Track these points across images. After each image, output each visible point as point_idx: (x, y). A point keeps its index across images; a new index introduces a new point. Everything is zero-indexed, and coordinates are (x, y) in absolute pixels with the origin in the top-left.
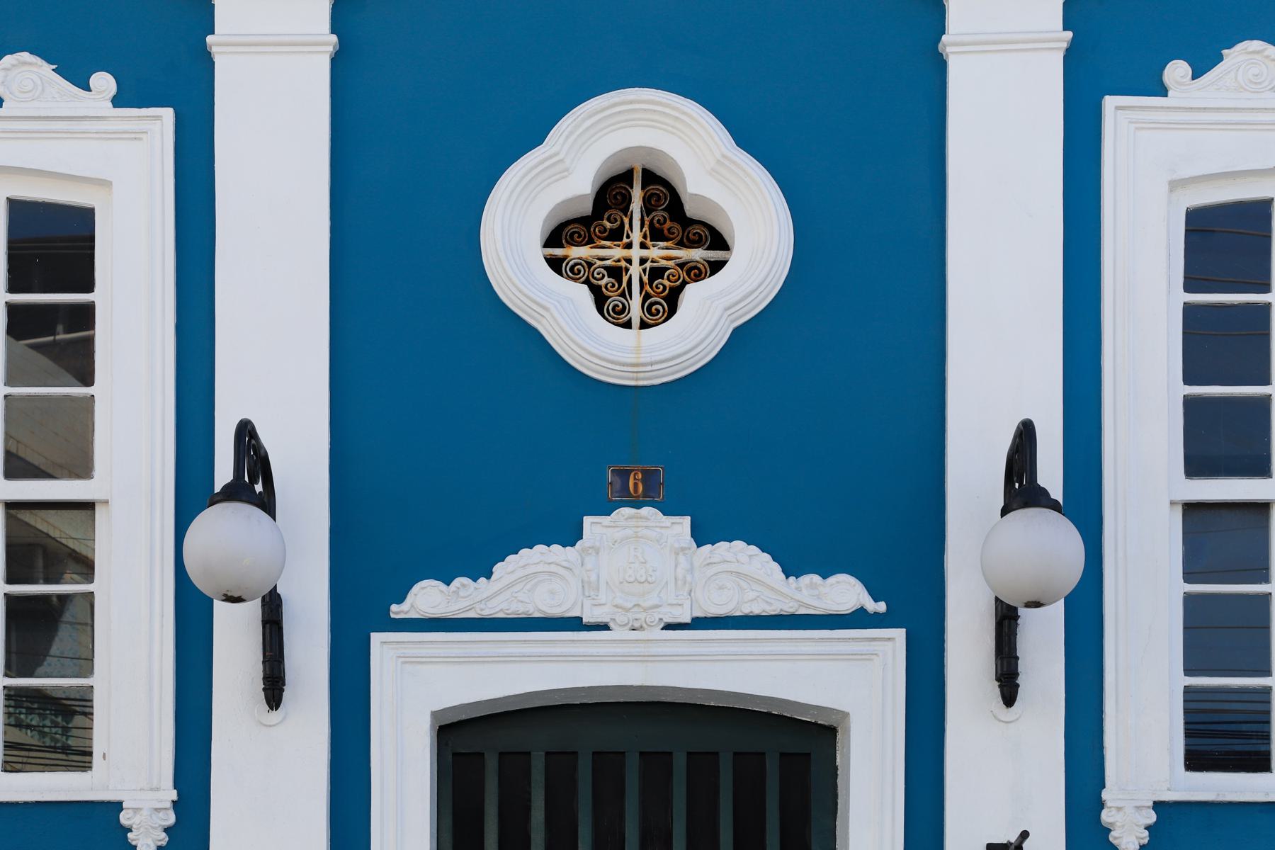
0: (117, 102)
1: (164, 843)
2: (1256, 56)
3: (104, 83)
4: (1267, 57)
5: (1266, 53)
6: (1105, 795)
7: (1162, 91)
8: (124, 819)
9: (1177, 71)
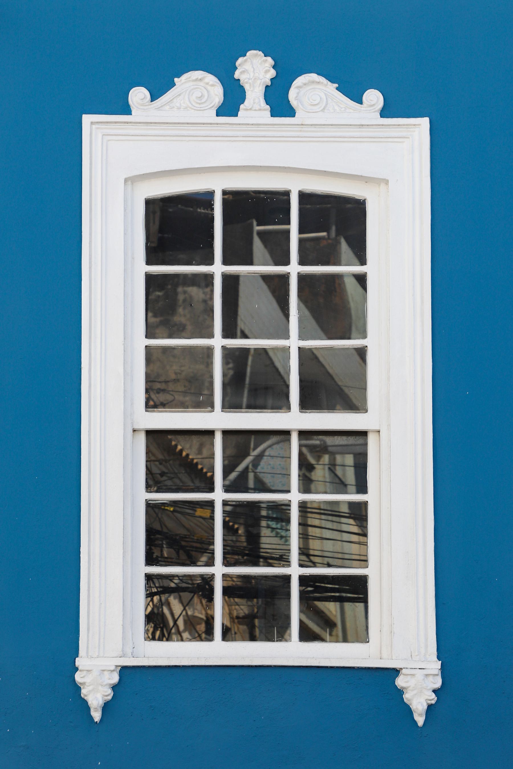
0: (385, 113)
1: (433, 702)
2: (199, 83)
3: (374, 98)
4: (207, 84)
5: (206, 80)
6: (79, 662)
7: (126, 110)
8: (400, 682)
9: (138, 95)
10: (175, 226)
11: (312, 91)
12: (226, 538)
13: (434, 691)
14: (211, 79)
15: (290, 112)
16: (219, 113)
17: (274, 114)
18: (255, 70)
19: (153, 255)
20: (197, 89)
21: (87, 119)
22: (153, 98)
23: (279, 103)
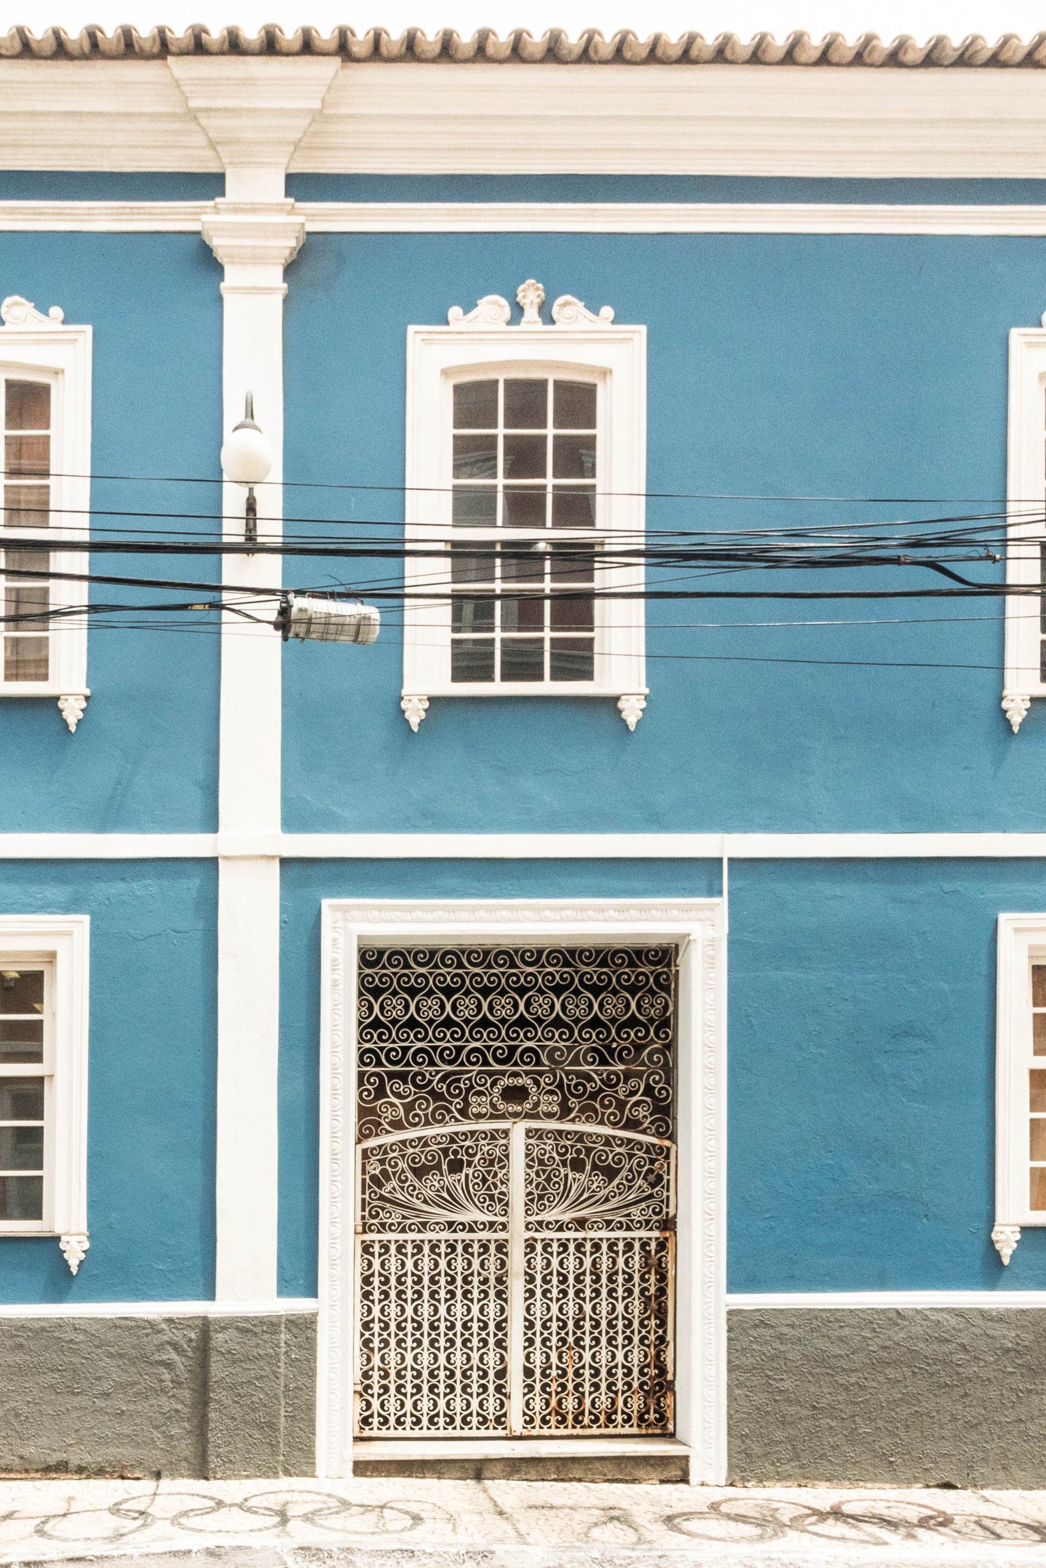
3: (607, 312)
9: (455, 312)
10: (472, 401)
11: (569, 309)
12: (303, 1380)
13: (642, 710)
14: (503, 301)
15: (553, 322)
16: (509, 323)
17: (544, 323)
18: (530, 294)
19: (457, 424)
20: (492, 308)
21: (411, 329)
22: (465, 313)
23: (546, 315)
